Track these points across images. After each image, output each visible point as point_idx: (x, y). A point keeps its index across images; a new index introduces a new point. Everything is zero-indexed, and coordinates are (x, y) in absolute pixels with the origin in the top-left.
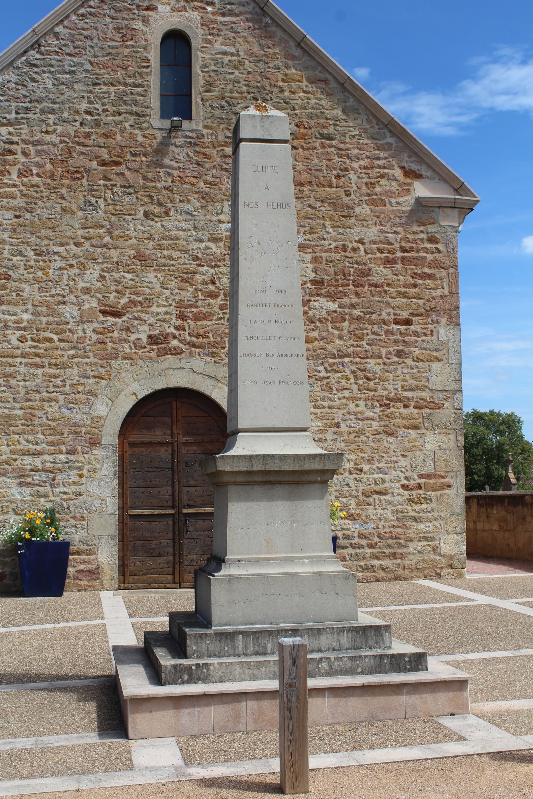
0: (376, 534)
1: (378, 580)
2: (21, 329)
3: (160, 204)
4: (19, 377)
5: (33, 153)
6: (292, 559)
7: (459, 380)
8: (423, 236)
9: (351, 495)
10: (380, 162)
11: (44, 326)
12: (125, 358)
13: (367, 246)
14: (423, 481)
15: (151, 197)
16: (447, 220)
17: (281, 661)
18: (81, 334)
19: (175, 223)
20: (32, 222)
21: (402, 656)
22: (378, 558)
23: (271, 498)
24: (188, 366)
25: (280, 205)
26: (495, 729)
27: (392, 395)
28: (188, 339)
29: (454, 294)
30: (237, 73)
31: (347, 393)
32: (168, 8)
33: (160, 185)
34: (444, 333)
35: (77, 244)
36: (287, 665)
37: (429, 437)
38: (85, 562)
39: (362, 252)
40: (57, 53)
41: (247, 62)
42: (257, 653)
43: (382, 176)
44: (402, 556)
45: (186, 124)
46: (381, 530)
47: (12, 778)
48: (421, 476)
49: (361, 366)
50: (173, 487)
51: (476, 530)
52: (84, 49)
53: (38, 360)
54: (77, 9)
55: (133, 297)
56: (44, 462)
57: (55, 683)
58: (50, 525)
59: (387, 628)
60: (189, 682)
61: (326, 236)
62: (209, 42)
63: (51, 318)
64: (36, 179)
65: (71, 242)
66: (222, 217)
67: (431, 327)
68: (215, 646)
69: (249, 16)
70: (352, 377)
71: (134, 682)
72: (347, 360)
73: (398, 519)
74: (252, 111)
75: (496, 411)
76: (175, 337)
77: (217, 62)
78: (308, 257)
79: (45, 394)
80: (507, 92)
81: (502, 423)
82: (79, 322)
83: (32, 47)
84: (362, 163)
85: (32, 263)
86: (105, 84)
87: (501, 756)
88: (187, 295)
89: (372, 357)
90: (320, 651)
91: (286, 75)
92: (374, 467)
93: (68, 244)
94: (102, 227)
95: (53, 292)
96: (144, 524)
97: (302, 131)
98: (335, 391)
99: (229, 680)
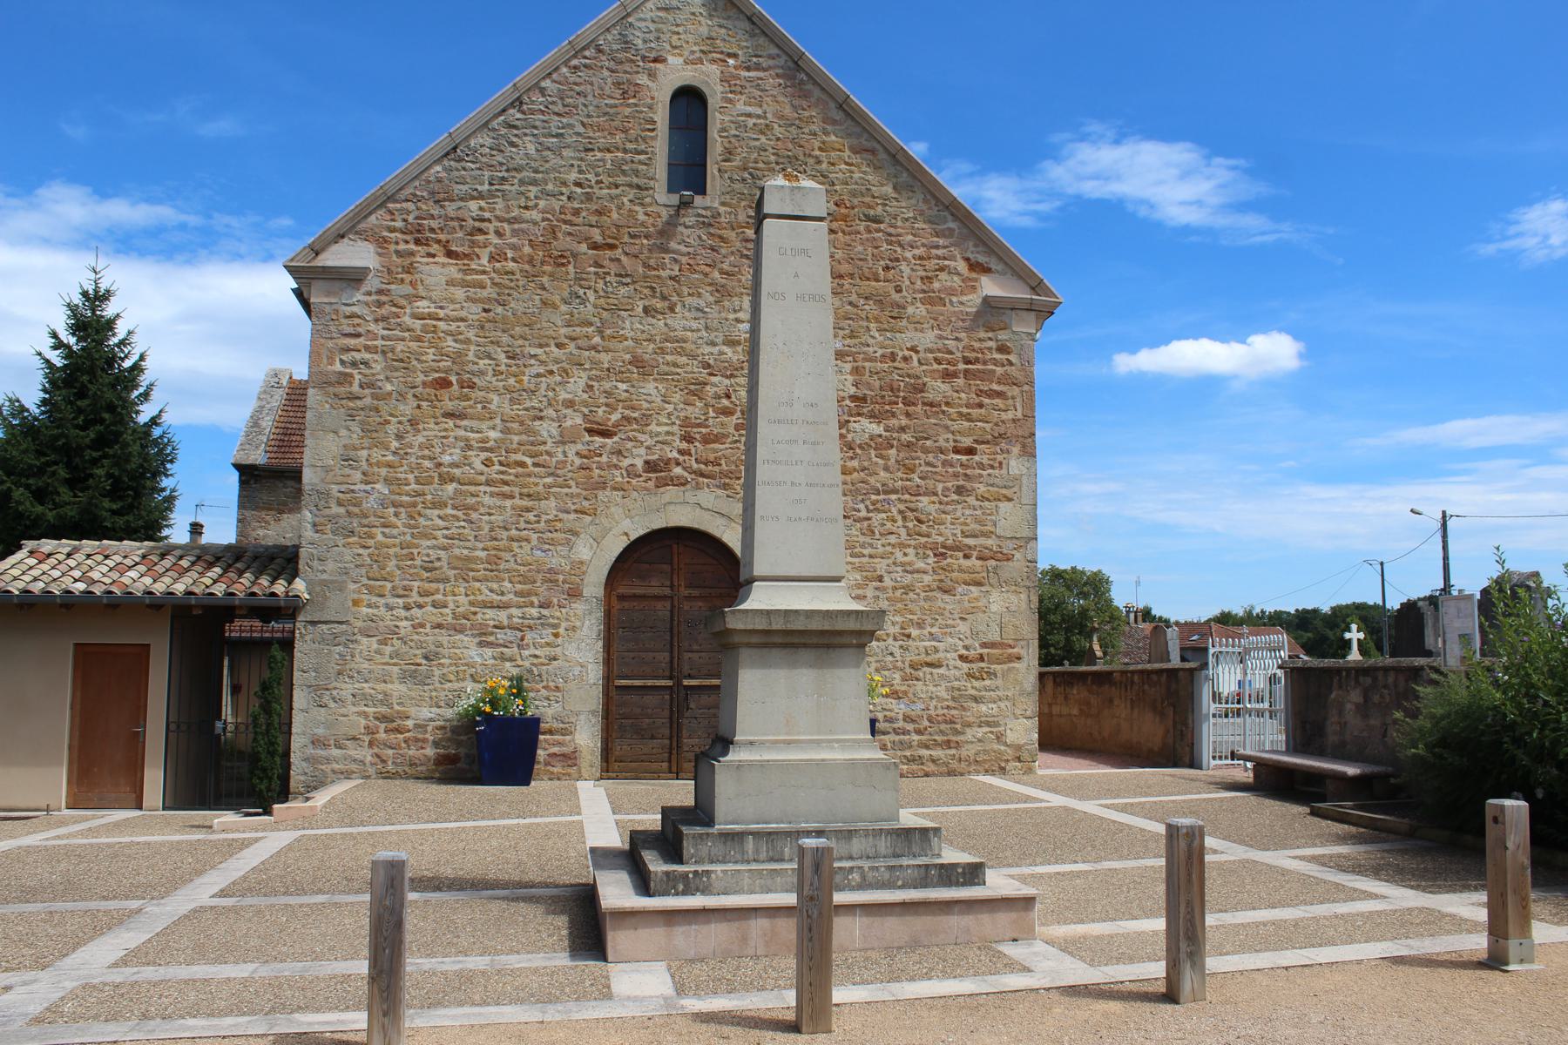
1: (927, 775)
3: (664, 298)
4: (482, 510)
5: (508, 233)
6: (818, 742)
7: (1033, 523)
8: (991, 344)
9: (895, 667)
10: (940, 252)
12: (615, 489)
13: (922, 355)
14: (986, 651)
15: (653, 289)
16: (1022, 326)
17: (800, 871)
18: (561, 457)
19: (681, 321)
20: (504, 317)
21: (954, 866)
22: (927, 747)
23: (793, 665)
24: (694, 500)
25: (813, 297)
26: (1068, 958)
27: (950, 542)
28: (695, 466)
29: (1029, 417)
30: (763, 139)
31: (893, 539)
32: (681, 60)
33: (664, 274)
34: (1015, 465)
35: (558, 346)
36: (808, 873)
37: (995, 596)
38: (559, 744)
39: (915, 363)
40: (543, 112)
42: (772, 860)
43: (942, 269)
44: (958, 745)
45: (698, 200)
46: (932, 712)
47: (461, 1004)
48: (984, 645)
49: (912, 505)
50: (672, 652)
51: (1050, 715)
52: (576, 107)
53: (506, 488)
54: (569, 60)
55: (627, 412)
56: (510, 617)
57: (519, 891)
58: (517, 696)
59: (937, 830)
60: (684, 893)
61: (871, 341)
62: (730, 101)
63: (524, 437)
64: (511, 264)
65: (552, 343)
66: (741, 315)
67: (999, 458)
68: (718, 849)
69: (780, 71)
70: (899, 518)
71: (616, 892)
72: (894, 497)
73: (953, 698)
74: (780, 181)
75: (1079, 568)
76: (678, 464)
77: (738, 125)
78: (848, 367)
79: (514, 532)
80: (1096, 177)
81: (1085, 584)
83: (512, 105)
84: (917, 252)
85: (503, 368)
86: (600, 150)
87: (1074, 991)
88: (695, 411)
89: (925, 494)
90: (851, 858)
92: (925, 632)
93: (547, 345)
94: (591, 324)
95: (528, 404)
96: (634, 698)
97: (843, 211)
99: (735, 892)
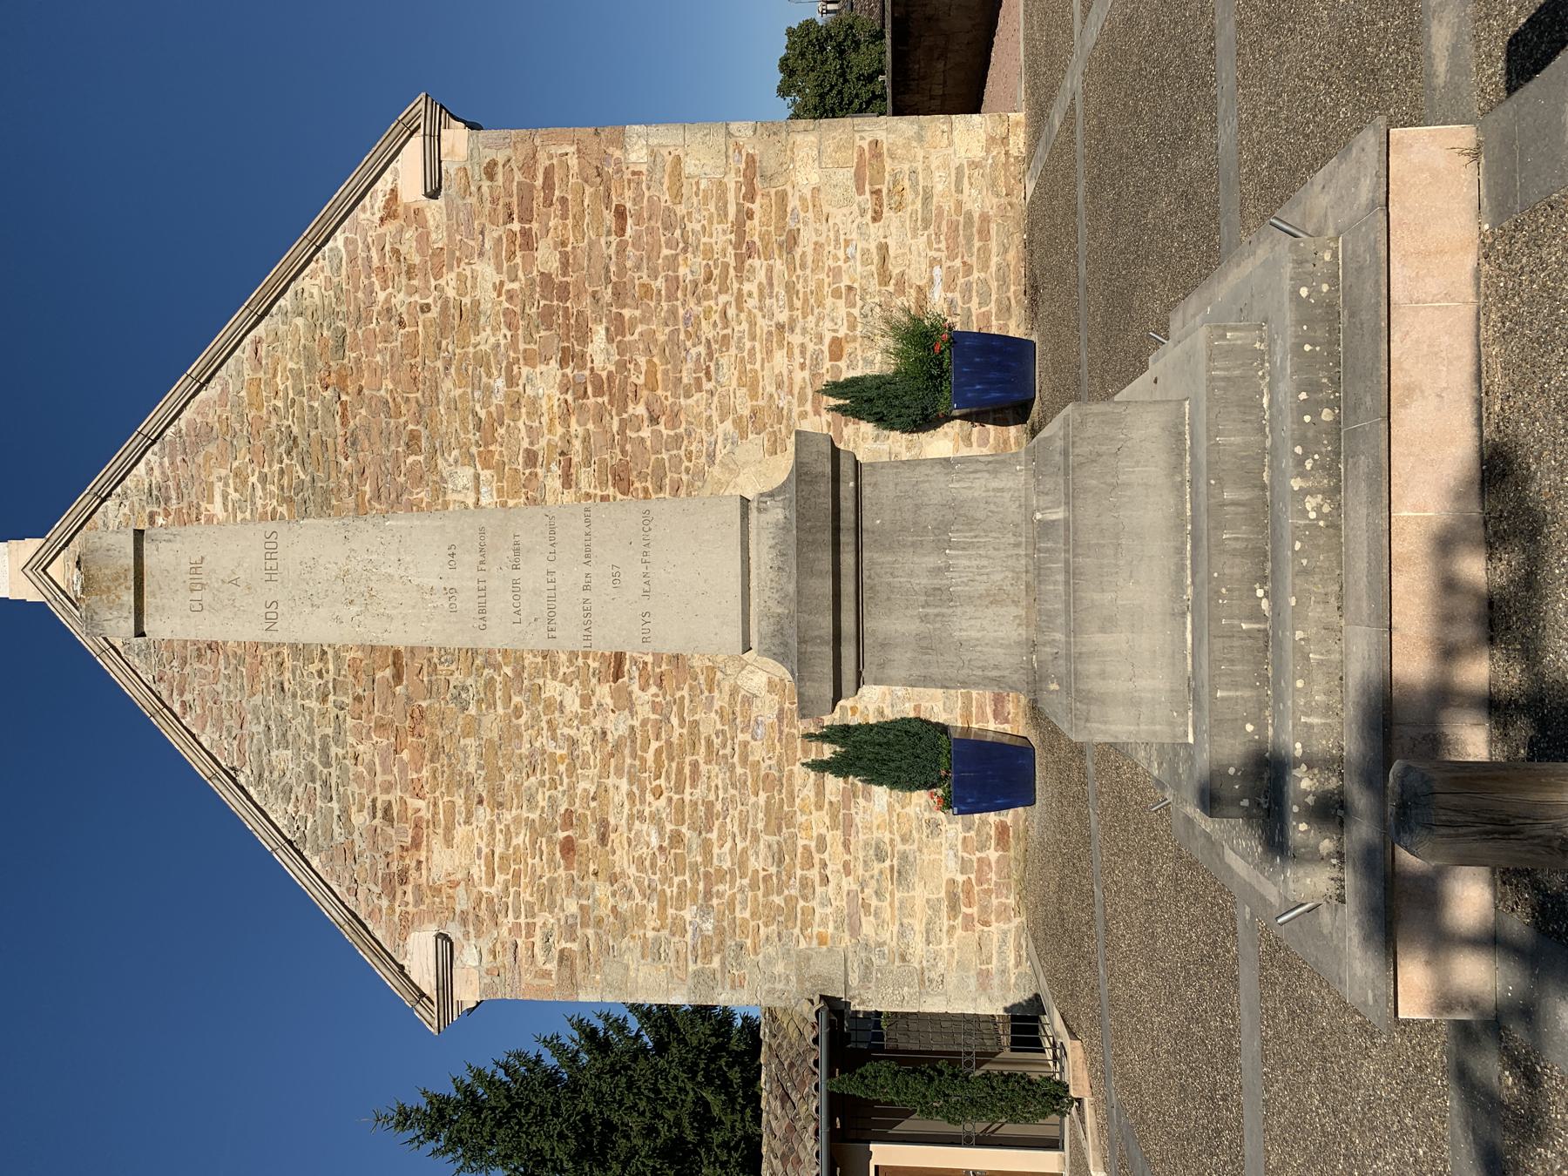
0: (949, 264)
2: (643, 792)
11: (637, 763)
14: (867, 187)
22: (988, 259)
31: (732, 312)
39: (516, 286)
41: (235, 464)
44: (985, 218)
67: (627, 175)
82: (631, 712)
91: (250, 404)
95: (588, 748)
98: (729, 331)
